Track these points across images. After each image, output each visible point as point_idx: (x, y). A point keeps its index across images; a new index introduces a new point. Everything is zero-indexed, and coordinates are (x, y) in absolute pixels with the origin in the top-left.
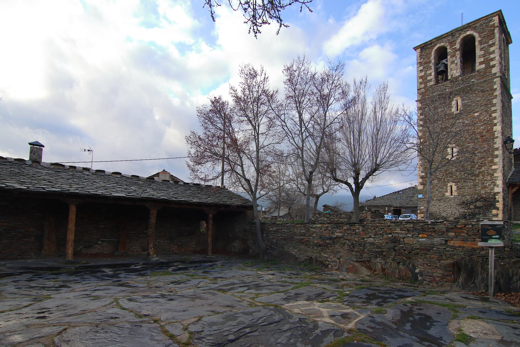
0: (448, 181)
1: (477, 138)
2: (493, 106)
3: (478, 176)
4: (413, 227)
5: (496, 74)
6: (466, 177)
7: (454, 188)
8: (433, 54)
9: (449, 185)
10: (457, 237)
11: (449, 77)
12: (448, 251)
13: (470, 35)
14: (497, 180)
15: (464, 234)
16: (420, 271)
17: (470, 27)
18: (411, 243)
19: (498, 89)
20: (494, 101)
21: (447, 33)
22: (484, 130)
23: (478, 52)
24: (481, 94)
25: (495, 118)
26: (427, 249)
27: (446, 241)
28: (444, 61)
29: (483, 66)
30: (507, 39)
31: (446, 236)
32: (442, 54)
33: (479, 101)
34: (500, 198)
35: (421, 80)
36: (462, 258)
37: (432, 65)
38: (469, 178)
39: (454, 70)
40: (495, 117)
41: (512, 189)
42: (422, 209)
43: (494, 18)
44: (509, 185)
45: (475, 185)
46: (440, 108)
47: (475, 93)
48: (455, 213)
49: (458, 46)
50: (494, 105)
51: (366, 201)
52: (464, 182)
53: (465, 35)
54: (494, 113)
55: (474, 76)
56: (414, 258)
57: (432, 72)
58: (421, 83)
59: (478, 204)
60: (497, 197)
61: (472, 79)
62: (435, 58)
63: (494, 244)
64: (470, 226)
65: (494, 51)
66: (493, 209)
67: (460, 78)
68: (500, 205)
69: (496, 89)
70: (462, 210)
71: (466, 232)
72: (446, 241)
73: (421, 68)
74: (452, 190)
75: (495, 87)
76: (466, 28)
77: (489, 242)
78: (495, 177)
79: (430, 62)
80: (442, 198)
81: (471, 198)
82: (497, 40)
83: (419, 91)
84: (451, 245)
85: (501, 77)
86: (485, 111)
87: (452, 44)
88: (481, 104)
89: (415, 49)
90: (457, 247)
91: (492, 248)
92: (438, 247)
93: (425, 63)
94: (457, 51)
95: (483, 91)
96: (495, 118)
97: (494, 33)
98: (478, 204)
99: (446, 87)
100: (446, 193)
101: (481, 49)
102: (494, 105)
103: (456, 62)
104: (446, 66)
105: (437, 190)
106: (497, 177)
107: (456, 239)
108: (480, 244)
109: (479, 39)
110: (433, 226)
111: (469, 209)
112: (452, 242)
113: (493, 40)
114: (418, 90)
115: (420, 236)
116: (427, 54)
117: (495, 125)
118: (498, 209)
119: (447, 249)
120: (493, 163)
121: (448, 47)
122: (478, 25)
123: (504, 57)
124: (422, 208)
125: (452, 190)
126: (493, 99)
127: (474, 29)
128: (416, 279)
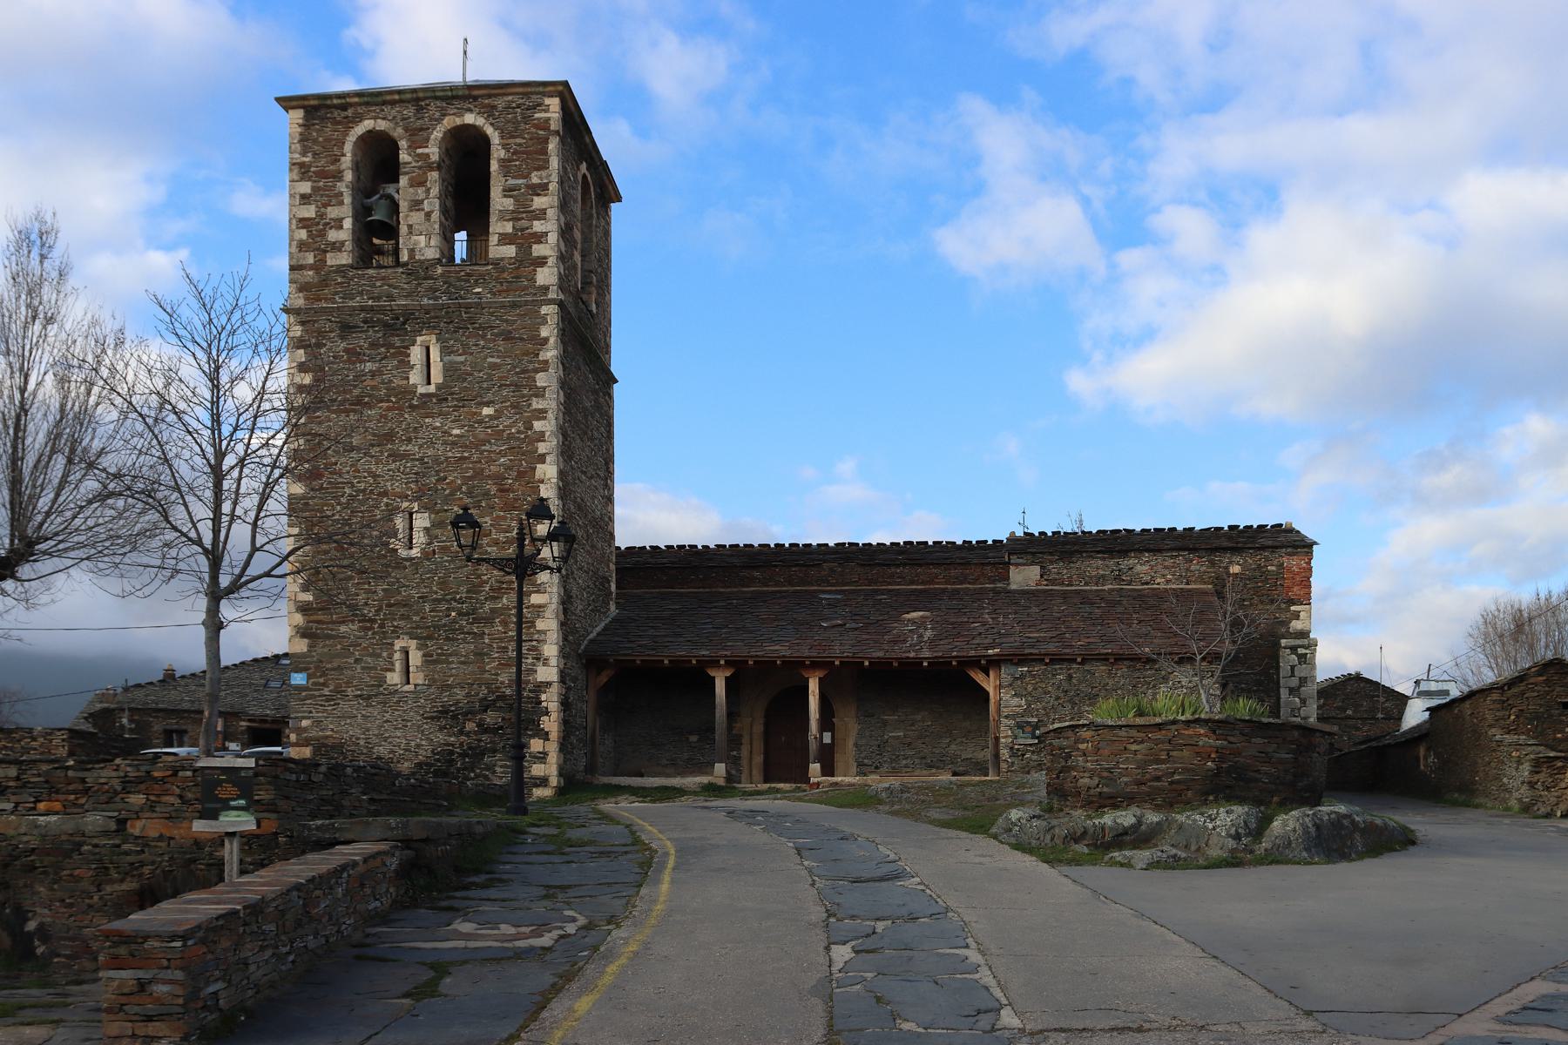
0: (396, 633)
1: (487, 494)
2: (537, 396)
3: (489, 621)
4: (18, 778)
5: (546, 289)
6: (454, 621)
7: (416, 658)
8: (348, 148)
9: (398, 644)
10: (152, 809)
11: (404, 257)
12: (126, 853)
13: (473, 126)
14: (544, 641)
15: (171, 799)
16: (41, 927)
17: (475, 98)
18: (11, 832)
19: (552, 340)
20: (541, 380)
21: (400, 92)
22: (509, 468)
23: (499, 201)
24: (502, 345)
25: (541, 437)
26: (63, 849)
27: (122, 823)
28: (390, 189)
29: (510, 251)
30: (594, 188)
31: (121, 806)
32: (380, 161)
33: (494, 366)
34: (551, 700)
35: (303, 234)
36: (166, 874)
37: (344, 187)
38: (461, 627)
39: (420, 236)
40: (542, 433)
41: (599, 674)
42: (305, 730)
43: (547, 101)
44: (583, 660)
45: (480, 655)
46: (371, 359)
47: (484, 337)
48: (418, 746)
49: (433, 151)
50: (540, 392)
51: (126, 689)
52: (447, 639)
53: (458, 121)
54: (539, 419)
55: (482, 276)
56: (21, 883)
57: (344, 212)
58: (302, 246)
59: (491, 718)
60: (543, 697)
61: (477, 284)
62: (356, 167)
63: (233, 824)
64: (189, 773)
65: (544, 211)
66: (533, 736)
67: (440, 270)
68: (551, 724)
69: (546, 340)
70: (441, 737)
71: (178, 791)
72: (122, 823)
73: (306, 187)
74: (407, 664)
75: (544, 333)
76: (464, 98)
77: (221, 818)
78: (539, 632)
79: (338, 176)
80: (377, 693)
81: (468, 695)
82: (555, 178)
83: (297, 275)
84: (137, 832)
85: (561, 304)
86: (513, 407)
87: (418, 136)
88: (501, 378)
89: (287, 103)
90: (154, 839)
91: (232, 835)
92: (95, 841)
93: (322, 174)
94: (432, 169)
95: (508, 337)
96: (541, 437)
97: (544, 152)
98: (491, 718)
99: (386, 287)
100: (389, 675)
101: (508, 191)
102: (540, 392)
103: (426, 206)
104: (394, 207)
105: (357, 661)
106: (544, 632)
107: (148, 815)
108: (199, 826)
109: (502, 154)
110: (80, 774)
111: (461, 732)
112: (139, 824)
113: (544, 173)
114: (292, 268)
115: (42, 806)
116: (327, 140)
117: (542, 459)
118: (545, 736)
119: (126, 847)
120: (534, 584)
121: (403, 144)
122: (500, 103)
123: (586, 240)
124: (305, 723)
125: (407, 664)
126: (537, 371)
127: (489, 112)
128: (29, 953)
